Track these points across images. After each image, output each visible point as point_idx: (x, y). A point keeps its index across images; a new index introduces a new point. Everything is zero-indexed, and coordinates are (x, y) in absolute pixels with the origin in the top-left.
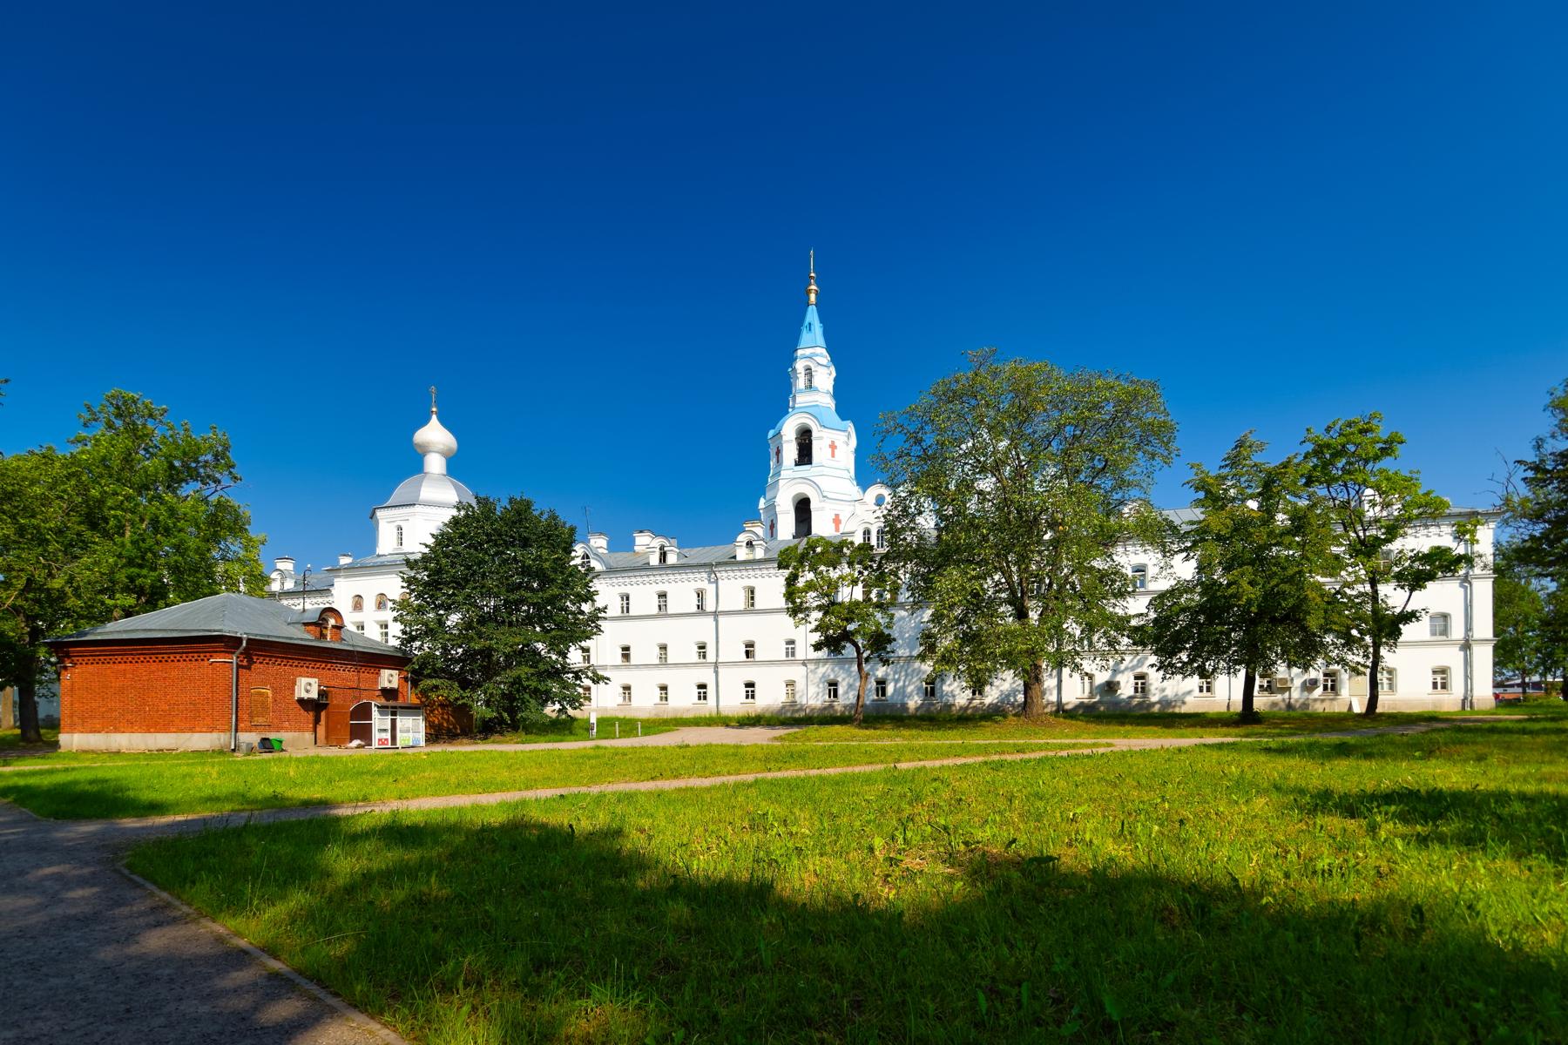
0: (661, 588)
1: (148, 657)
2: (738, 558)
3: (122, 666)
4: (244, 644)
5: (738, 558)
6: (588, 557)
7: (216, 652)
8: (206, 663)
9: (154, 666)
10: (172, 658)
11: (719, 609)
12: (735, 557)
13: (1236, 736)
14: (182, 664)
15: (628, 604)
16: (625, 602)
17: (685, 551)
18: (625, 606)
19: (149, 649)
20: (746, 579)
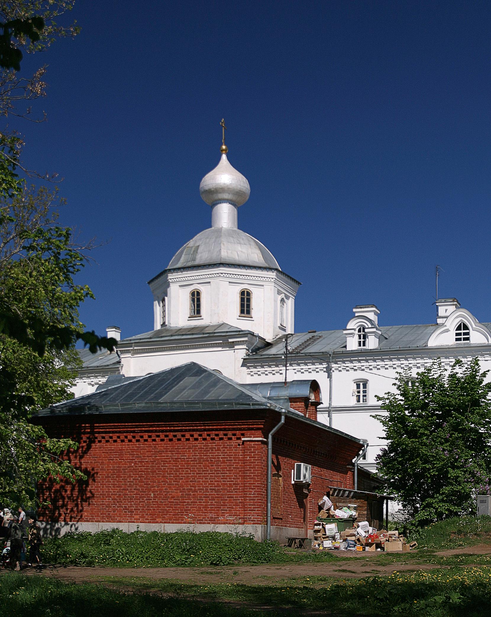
0: (360, 375)
1: (154, 435)
2: (349, 348)
3: (119, 445)
4: (283, 421)
5: (349, 348)
6: (466, 327)
7: (252, 429)
8: (234, 442)
9: (161, 446)
10: (146, 437)
11: (334, 404)
12: (345, 347)
13: (413, 564)
14: (200, 444)
15: (365, 392)
16: (362, 389)
17: (392, 331)
18: (361, 394)
19: (158, 426)
20: (256, 376)
